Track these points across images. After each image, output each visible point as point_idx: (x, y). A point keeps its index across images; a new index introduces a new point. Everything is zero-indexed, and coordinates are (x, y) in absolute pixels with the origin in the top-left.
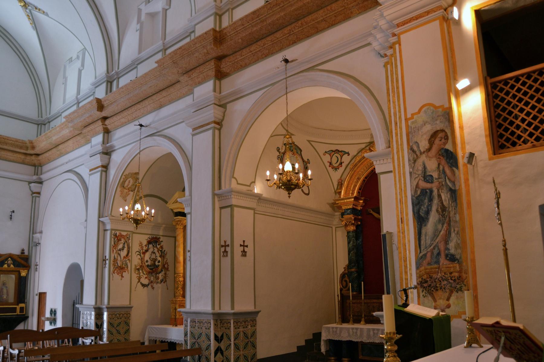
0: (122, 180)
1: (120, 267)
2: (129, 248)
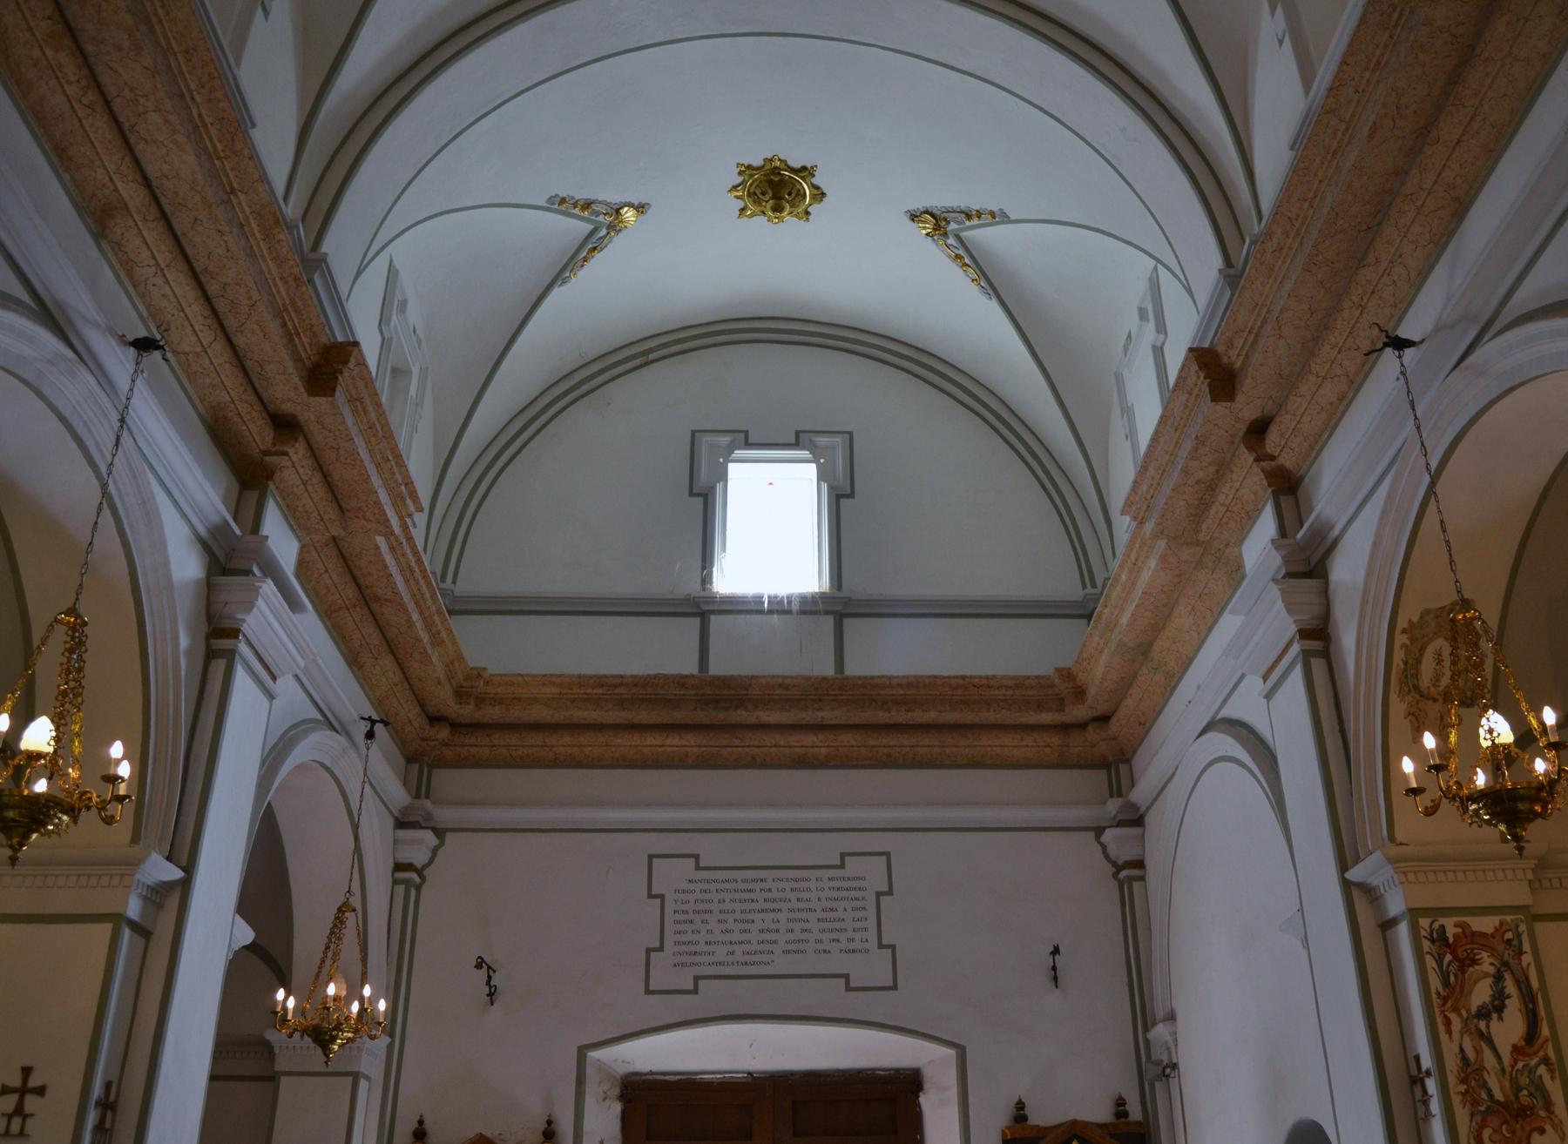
0: (1399, 655)
1: (1505, 1105)
2: (1523, 984)
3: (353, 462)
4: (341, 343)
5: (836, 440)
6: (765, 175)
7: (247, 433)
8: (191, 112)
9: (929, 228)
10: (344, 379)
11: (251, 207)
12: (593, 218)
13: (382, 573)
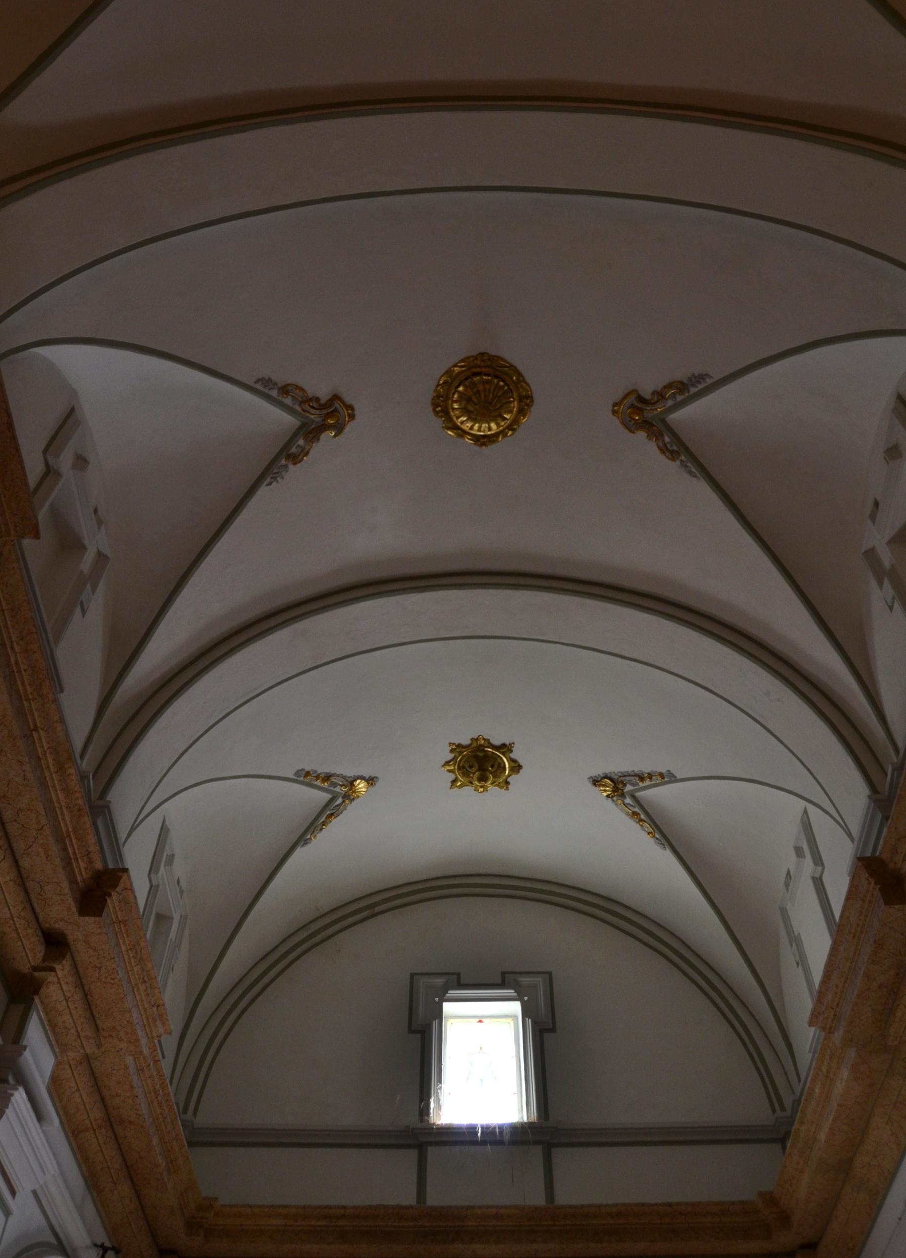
3: (112, 981)
4: (113, 870)
5: (537, 979)
6: (472, 752)
7: (21, 949)
8: (10, 659)
9: (608, 791)
10: (113, 901)
11: (48, 743)
12: (332, 788)
13: (128, 1094)
